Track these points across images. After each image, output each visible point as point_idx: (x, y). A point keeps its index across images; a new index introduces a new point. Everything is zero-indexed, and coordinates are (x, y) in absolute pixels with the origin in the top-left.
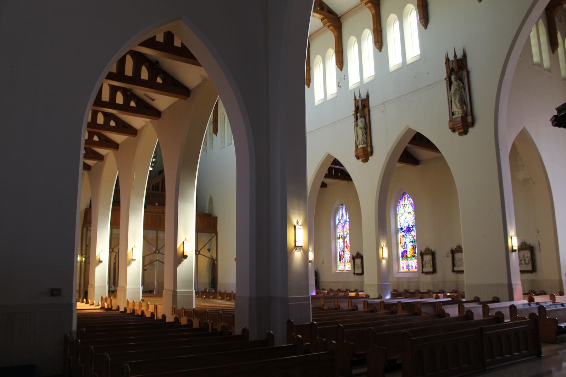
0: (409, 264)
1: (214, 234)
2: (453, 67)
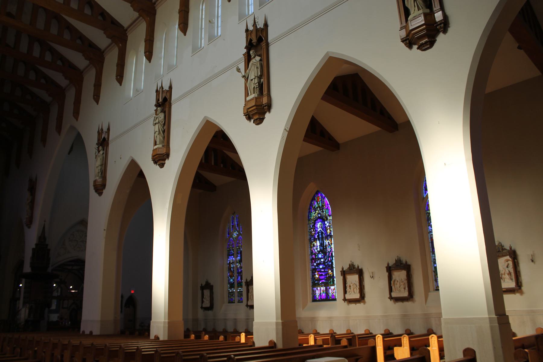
2: (251, 38)
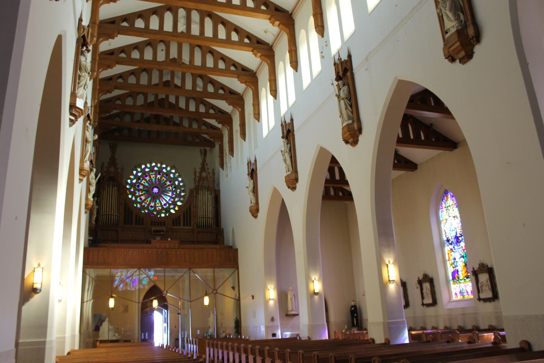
0: (463, 289)
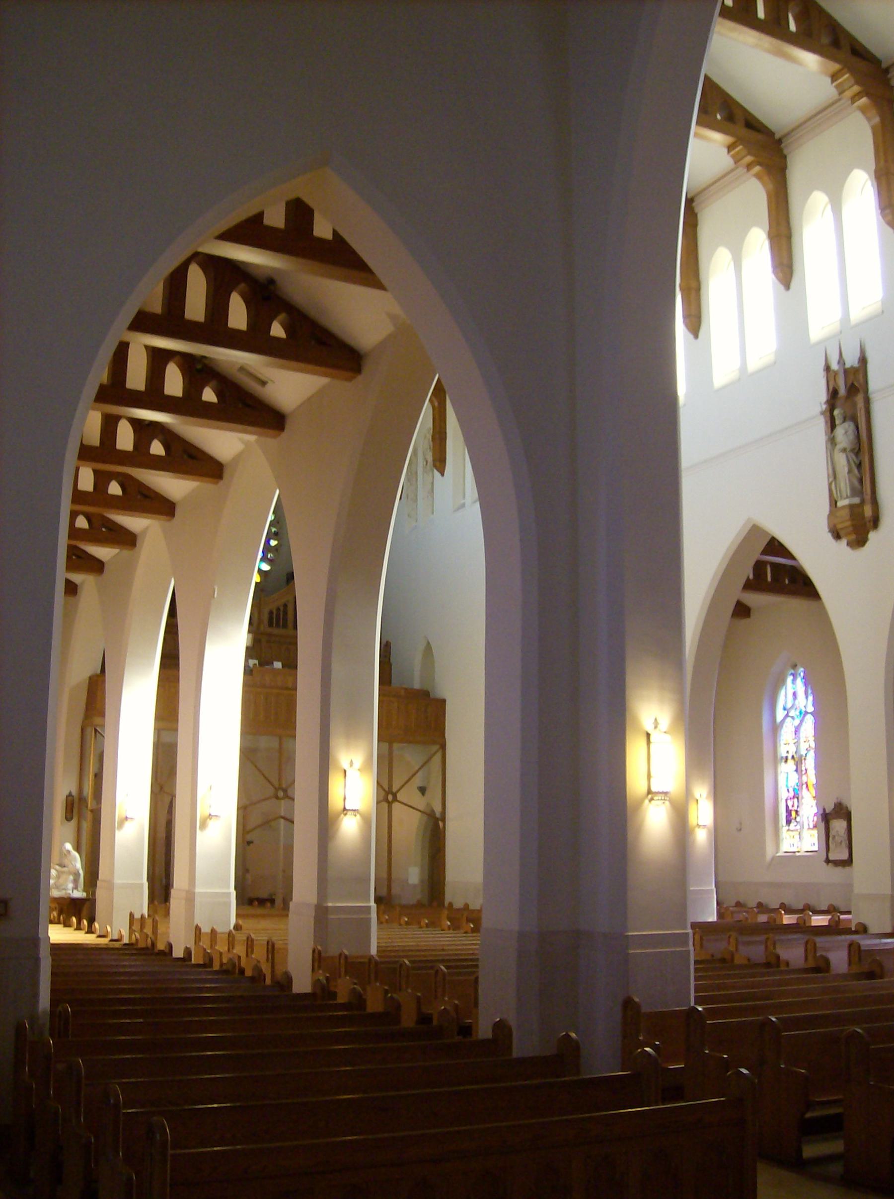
1: (435, 748)
